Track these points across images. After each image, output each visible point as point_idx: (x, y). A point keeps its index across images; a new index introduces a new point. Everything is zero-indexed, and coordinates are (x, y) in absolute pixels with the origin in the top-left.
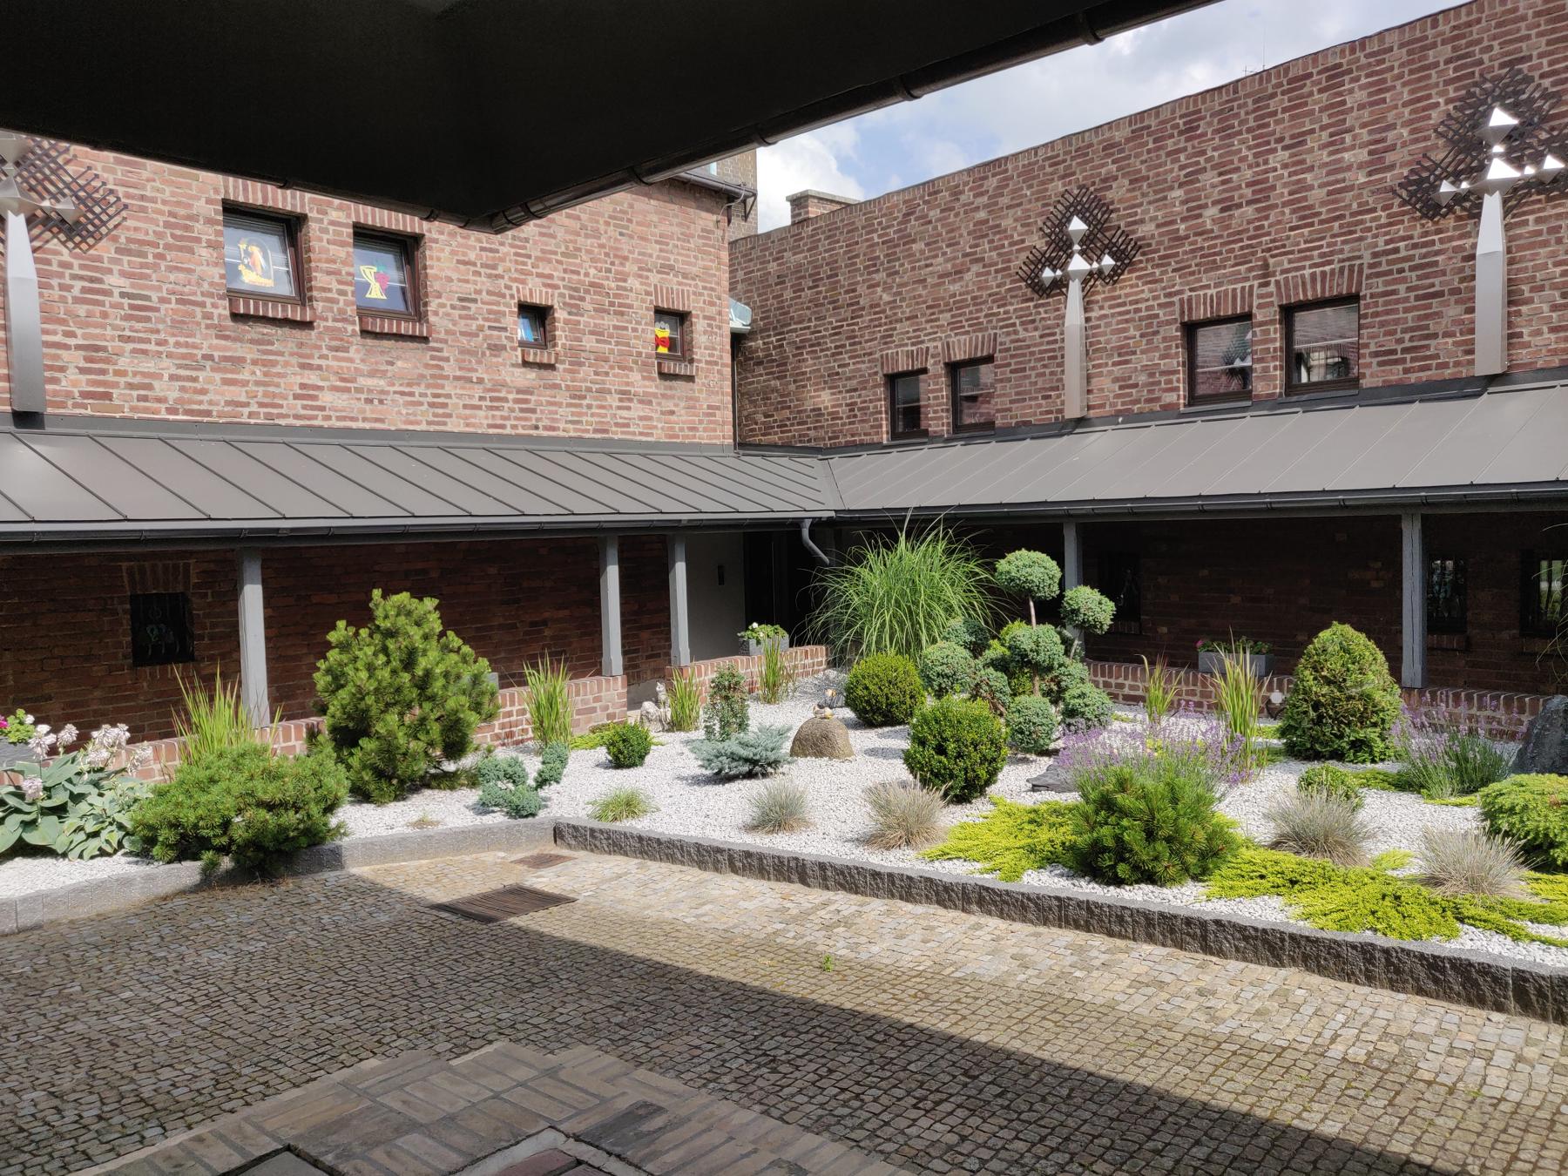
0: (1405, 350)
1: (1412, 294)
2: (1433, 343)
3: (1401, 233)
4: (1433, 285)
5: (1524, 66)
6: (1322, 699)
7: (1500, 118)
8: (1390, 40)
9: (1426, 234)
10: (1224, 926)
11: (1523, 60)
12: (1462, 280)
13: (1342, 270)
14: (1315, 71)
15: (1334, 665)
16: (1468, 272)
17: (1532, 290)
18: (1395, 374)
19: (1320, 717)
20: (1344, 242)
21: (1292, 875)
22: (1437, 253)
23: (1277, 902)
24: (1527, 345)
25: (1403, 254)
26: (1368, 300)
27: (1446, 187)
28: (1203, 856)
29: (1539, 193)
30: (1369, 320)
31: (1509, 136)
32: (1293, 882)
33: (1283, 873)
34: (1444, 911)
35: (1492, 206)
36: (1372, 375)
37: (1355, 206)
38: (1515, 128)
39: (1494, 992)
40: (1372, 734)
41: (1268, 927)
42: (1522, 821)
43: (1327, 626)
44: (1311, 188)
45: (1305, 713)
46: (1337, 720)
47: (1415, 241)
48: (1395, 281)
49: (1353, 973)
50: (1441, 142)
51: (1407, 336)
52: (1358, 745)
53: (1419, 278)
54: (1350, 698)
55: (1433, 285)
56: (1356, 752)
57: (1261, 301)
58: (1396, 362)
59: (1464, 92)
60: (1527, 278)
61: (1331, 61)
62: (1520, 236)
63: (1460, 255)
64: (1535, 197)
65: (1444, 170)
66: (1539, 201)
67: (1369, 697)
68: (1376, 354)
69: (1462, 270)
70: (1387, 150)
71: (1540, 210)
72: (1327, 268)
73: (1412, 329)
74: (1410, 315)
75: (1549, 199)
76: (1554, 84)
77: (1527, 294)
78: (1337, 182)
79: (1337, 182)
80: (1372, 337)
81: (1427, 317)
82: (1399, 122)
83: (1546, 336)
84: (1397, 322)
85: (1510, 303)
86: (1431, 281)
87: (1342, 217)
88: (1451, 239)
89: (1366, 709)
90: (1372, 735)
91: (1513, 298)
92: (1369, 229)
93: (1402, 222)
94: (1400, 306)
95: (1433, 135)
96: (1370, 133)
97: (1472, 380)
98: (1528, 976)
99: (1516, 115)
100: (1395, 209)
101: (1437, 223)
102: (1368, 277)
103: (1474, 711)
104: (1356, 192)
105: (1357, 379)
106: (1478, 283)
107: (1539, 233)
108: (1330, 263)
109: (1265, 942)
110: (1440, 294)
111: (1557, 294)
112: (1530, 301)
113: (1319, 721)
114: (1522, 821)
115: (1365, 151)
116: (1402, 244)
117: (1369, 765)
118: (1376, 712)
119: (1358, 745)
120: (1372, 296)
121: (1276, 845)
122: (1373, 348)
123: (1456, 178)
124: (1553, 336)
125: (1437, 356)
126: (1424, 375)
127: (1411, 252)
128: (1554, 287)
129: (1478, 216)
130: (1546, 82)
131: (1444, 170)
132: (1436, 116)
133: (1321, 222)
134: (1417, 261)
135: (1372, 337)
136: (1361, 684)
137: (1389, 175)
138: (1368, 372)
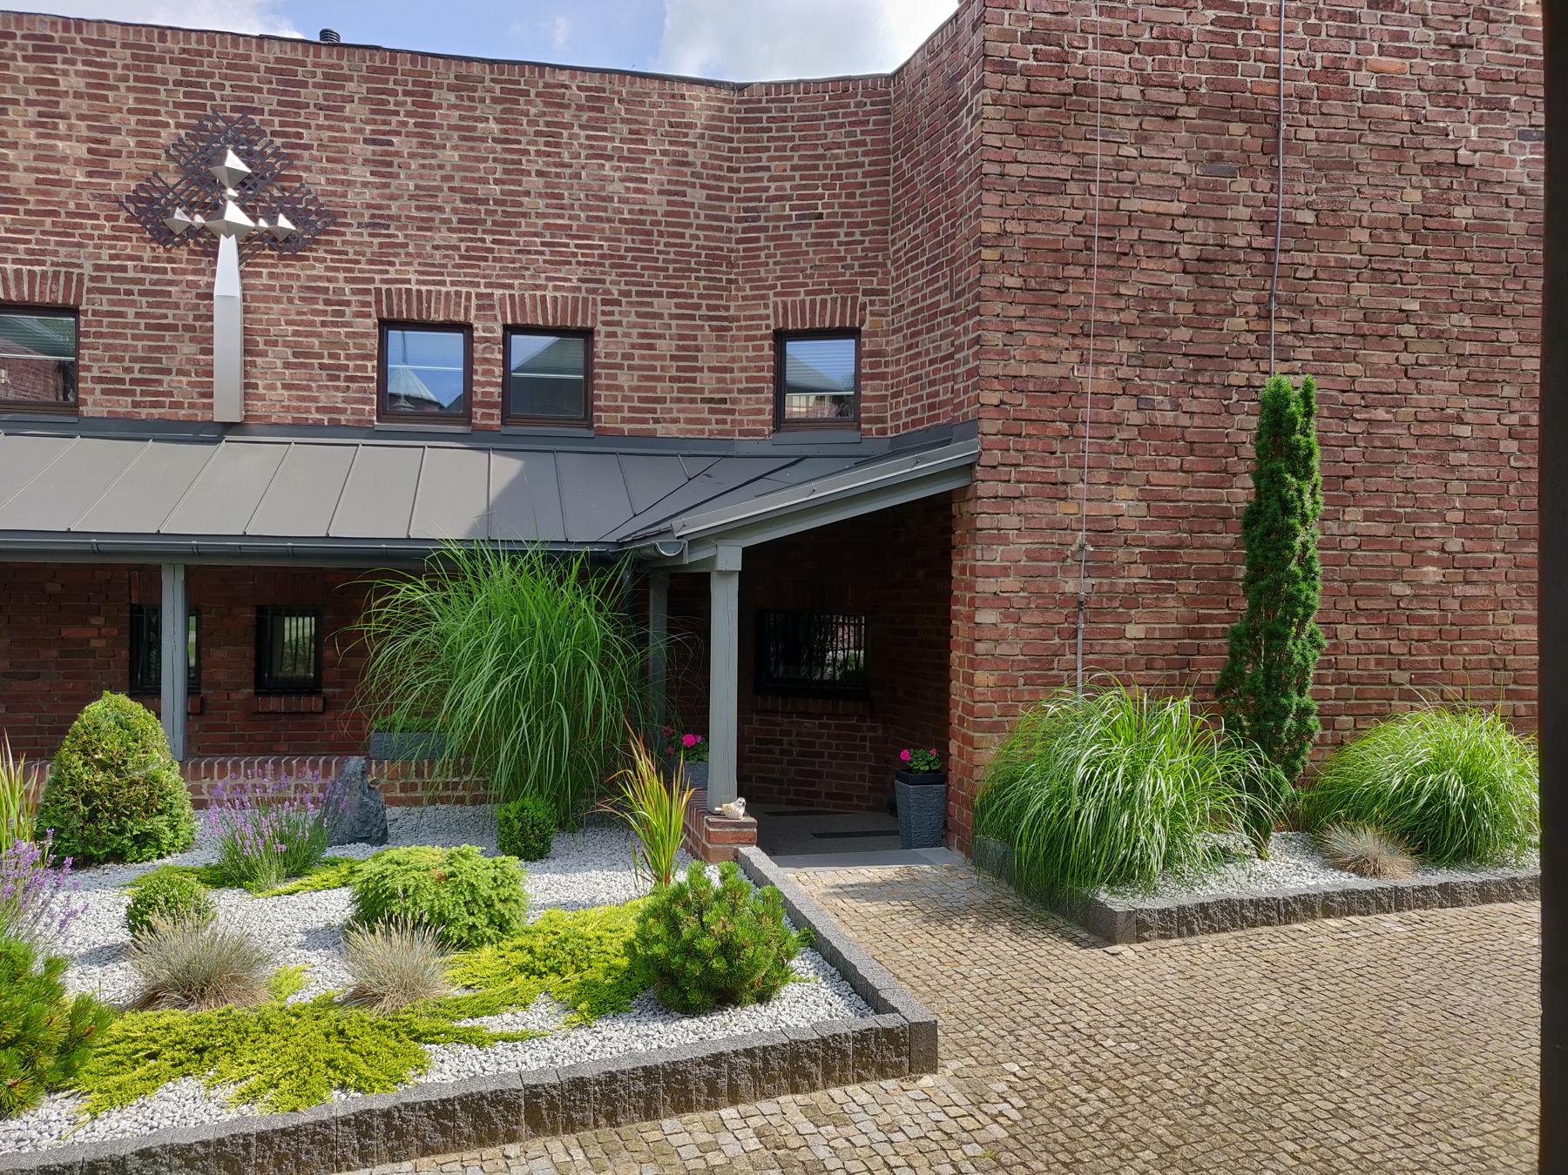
0: (133, 381)
1: (142, 322)
2: (166, 378)
3: (129, 251)
4: (166, 317)
5: (257, 118)
6: (97, 789)
7: (233, 161)
8: (112, 34)
9: (156, 259)
10: (154, 1155)
11: (254, 111)
12: (197, 318)
13: (56, 275)
14: (19, 33)
15: (111, 744)
16: (203, 311)
17: (266, 343)
18: (123, 405)
19: (94, 811)
20: (58, 243)
21: (197, 1041)
22: (171, 283)
23: (188, 1086)
24: (262, 398)
25: (131, 274)
26: (90, 317)
27: (179, 215)
28: (65, 1050)
29: (272, 248)
30: (91, 340)
31: (242, 182)
32: (200, 1051)
33: (182, 1042)
34: (397, 1035)
35: (228, 248)
36: (94, 403)
37: (72, 206)
38: (249, 177)
39: (506, 1121)
40: (160, 823)
41: (223, 1134)
42: (415, 904)
43: (96, 697)
44: (14, 168)
45: (74, 808)
46: (116, 812)
47: (145, 263)
48: (121, 303)
49: (345, 1158)
50: (172, 166)
51: (137, 366)
52: (142, 840)
53: (150, 305)
54: (133, 783)
55: (166, 317)
56: (140, 848)
57: (11, 276)
58: (124, 393)
59: (195, 122)
60: (262, 330)
61: (39, 30)
62: (254, 287)
63: (194, 291)
64: (267, 252)
65: (177, 196)
66: (272, 257)
67: (155, 779)
68: (100, 380)
69: (196, 307)
70: (111, 154)
71: (273, 265)
72: (37, 268)
73: (142, 360)
74: (140, 344)
75: (281, 258)
76: (285, 145)
77: (261, 347)
78: (49, 171)
79: (49, 171)
80: (94, 359)
81: (158, 349)
82: (124, 128)
83: (280, 391)
84: (125, 348)
85: (246, 352)
86: (163, 311)
87: (55, 213)
88: (184, 272)
89: (151, 794)
90: (161, 825)
91: (249, 349)
92: (91, 237)
93: (130, 239)
94: (129, 332)
95: (164, 155)
96: (138, 122)
97: (211, 424)
98: (540, 1089)
99: (249, 165)
100: (121, 223)
101: (169, 251)
102: (89, 291)
103: (241, 780)
104: (73, 189)
105: (76, 405)
106: (217, 323)
107: (272, 288)
108: (42, 263)
109: (221, 1157)
110: (173, 328)
111: (289, 352)
112: (263, 354)
113: (92, 817)
114: (415, 904)
115: (84, 147)
116: (130, 264)
117: (156, 862)
118: (162, 797)
119: (142, 840)
120: (95, 313)
121: (149, 1000)
122: (96, 373)
123: (190, 208)
124: (286, 393)
125: (170, 394)
126: (156, 412)
127: (142, 275)
128: (287, 344)
129: (216, 255)
130: (278, 141)
131: (177, 196)
132: (166, 137)
133: (28, 212)
134: (147, 286)
135: (94, 359)
136: (146, 765)
137: (113, 183)
138: (90, 399)
